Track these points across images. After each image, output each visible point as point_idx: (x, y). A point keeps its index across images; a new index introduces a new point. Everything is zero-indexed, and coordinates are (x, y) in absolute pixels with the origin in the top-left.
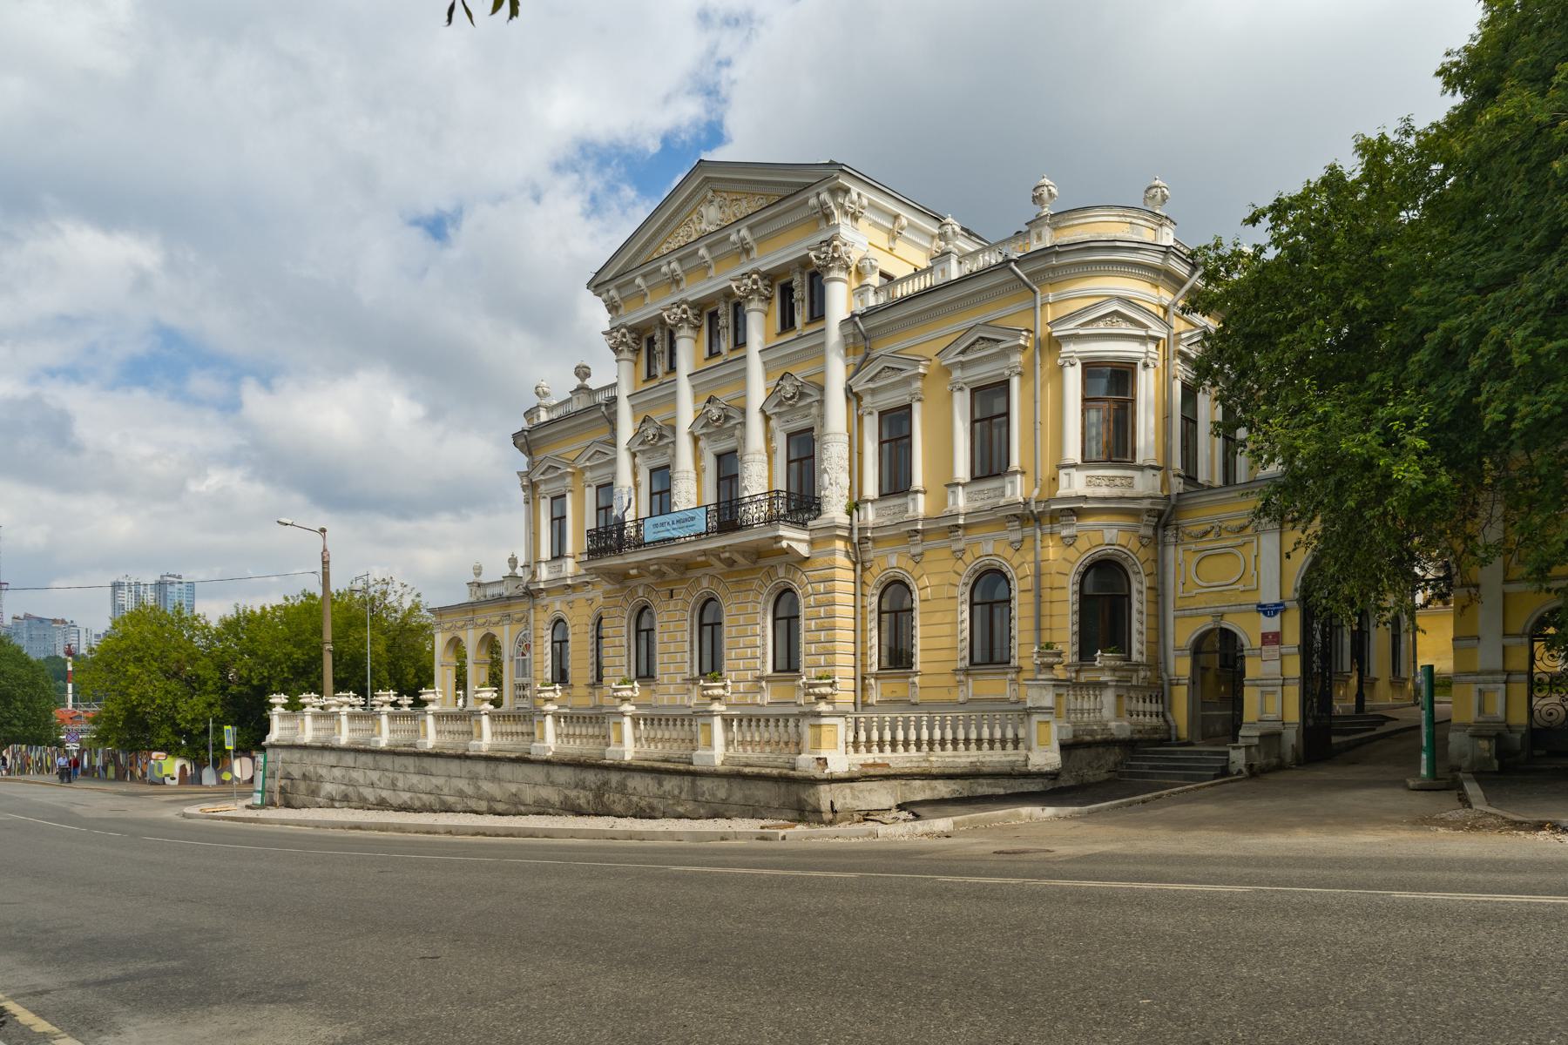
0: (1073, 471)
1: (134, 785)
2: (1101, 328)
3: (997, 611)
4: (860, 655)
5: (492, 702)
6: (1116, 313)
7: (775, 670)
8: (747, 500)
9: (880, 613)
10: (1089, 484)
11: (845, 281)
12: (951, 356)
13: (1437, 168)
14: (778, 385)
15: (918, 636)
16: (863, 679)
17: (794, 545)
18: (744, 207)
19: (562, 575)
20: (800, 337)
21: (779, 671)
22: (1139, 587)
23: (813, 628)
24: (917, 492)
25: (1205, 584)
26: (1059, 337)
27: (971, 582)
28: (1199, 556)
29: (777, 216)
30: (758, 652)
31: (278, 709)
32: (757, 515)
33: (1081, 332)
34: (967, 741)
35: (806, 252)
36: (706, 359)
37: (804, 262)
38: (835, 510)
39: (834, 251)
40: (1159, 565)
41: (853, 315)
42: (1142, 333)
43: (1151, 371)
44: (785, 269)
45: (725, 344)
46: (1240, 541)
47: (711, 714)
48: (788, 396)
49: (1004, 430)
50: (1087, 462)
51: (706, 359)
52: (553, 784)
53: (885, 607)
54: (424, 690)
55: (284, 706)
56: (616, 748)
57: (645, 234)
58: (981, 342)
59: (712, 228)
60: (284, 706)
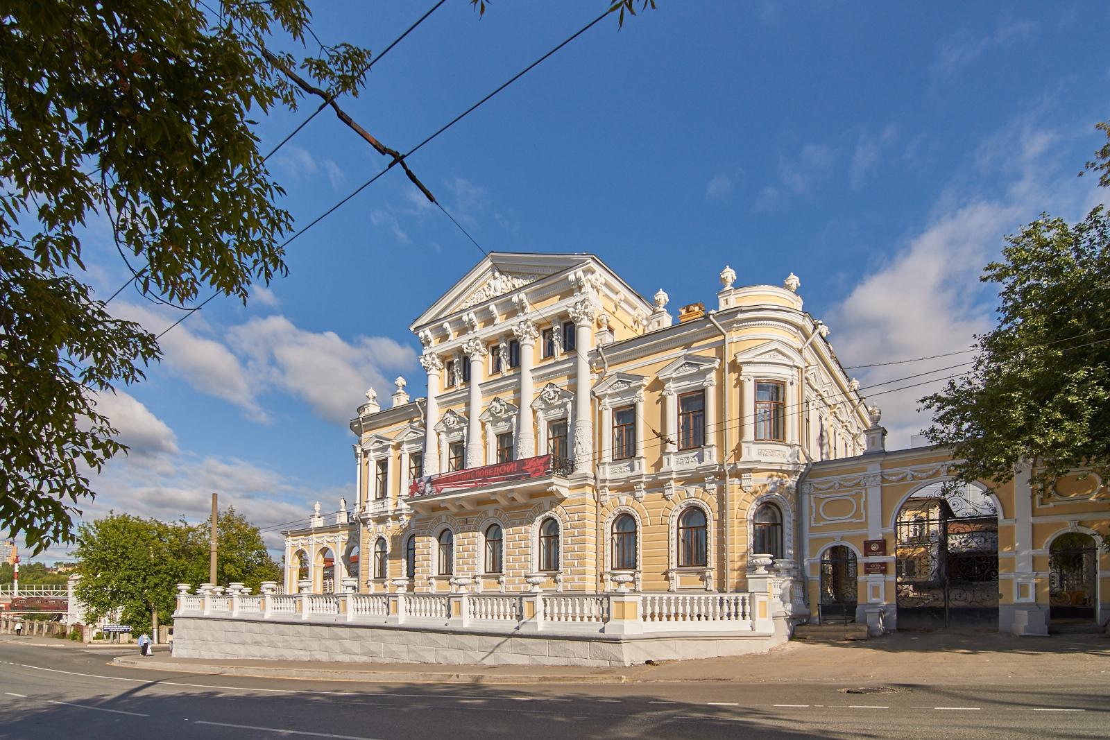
0: (751, 444)
1: (50, 640)
2: (766, 358)
4: (599, 559)
5: (354, 588)
6: (776, 350)
7: (678, 566)
10: (760, 453)
11: (590, 328)
13: (65, 426)
16: (602, 575)
17: (559, 488)
18: (519, 283)
19: (385, 509)
20: (557, 363)
21: (615, 569)
22: (789, 519)
24: (670, 453)
31: (184, 592)
33: (756, 361)
34: (676, 615)
35: (566, 308)
37: (563, 316)
38: (584, 466)
39: (585, 308)
43: (794, 386)
44: (550, 321)
47: (461, 596)
49: (632, 432)
51: (446, 389)
53: (681, 526)
55: (188, 591)
56: (455, 619)
57: (451, 296)
59: (498, 294)
60: (188, 591)
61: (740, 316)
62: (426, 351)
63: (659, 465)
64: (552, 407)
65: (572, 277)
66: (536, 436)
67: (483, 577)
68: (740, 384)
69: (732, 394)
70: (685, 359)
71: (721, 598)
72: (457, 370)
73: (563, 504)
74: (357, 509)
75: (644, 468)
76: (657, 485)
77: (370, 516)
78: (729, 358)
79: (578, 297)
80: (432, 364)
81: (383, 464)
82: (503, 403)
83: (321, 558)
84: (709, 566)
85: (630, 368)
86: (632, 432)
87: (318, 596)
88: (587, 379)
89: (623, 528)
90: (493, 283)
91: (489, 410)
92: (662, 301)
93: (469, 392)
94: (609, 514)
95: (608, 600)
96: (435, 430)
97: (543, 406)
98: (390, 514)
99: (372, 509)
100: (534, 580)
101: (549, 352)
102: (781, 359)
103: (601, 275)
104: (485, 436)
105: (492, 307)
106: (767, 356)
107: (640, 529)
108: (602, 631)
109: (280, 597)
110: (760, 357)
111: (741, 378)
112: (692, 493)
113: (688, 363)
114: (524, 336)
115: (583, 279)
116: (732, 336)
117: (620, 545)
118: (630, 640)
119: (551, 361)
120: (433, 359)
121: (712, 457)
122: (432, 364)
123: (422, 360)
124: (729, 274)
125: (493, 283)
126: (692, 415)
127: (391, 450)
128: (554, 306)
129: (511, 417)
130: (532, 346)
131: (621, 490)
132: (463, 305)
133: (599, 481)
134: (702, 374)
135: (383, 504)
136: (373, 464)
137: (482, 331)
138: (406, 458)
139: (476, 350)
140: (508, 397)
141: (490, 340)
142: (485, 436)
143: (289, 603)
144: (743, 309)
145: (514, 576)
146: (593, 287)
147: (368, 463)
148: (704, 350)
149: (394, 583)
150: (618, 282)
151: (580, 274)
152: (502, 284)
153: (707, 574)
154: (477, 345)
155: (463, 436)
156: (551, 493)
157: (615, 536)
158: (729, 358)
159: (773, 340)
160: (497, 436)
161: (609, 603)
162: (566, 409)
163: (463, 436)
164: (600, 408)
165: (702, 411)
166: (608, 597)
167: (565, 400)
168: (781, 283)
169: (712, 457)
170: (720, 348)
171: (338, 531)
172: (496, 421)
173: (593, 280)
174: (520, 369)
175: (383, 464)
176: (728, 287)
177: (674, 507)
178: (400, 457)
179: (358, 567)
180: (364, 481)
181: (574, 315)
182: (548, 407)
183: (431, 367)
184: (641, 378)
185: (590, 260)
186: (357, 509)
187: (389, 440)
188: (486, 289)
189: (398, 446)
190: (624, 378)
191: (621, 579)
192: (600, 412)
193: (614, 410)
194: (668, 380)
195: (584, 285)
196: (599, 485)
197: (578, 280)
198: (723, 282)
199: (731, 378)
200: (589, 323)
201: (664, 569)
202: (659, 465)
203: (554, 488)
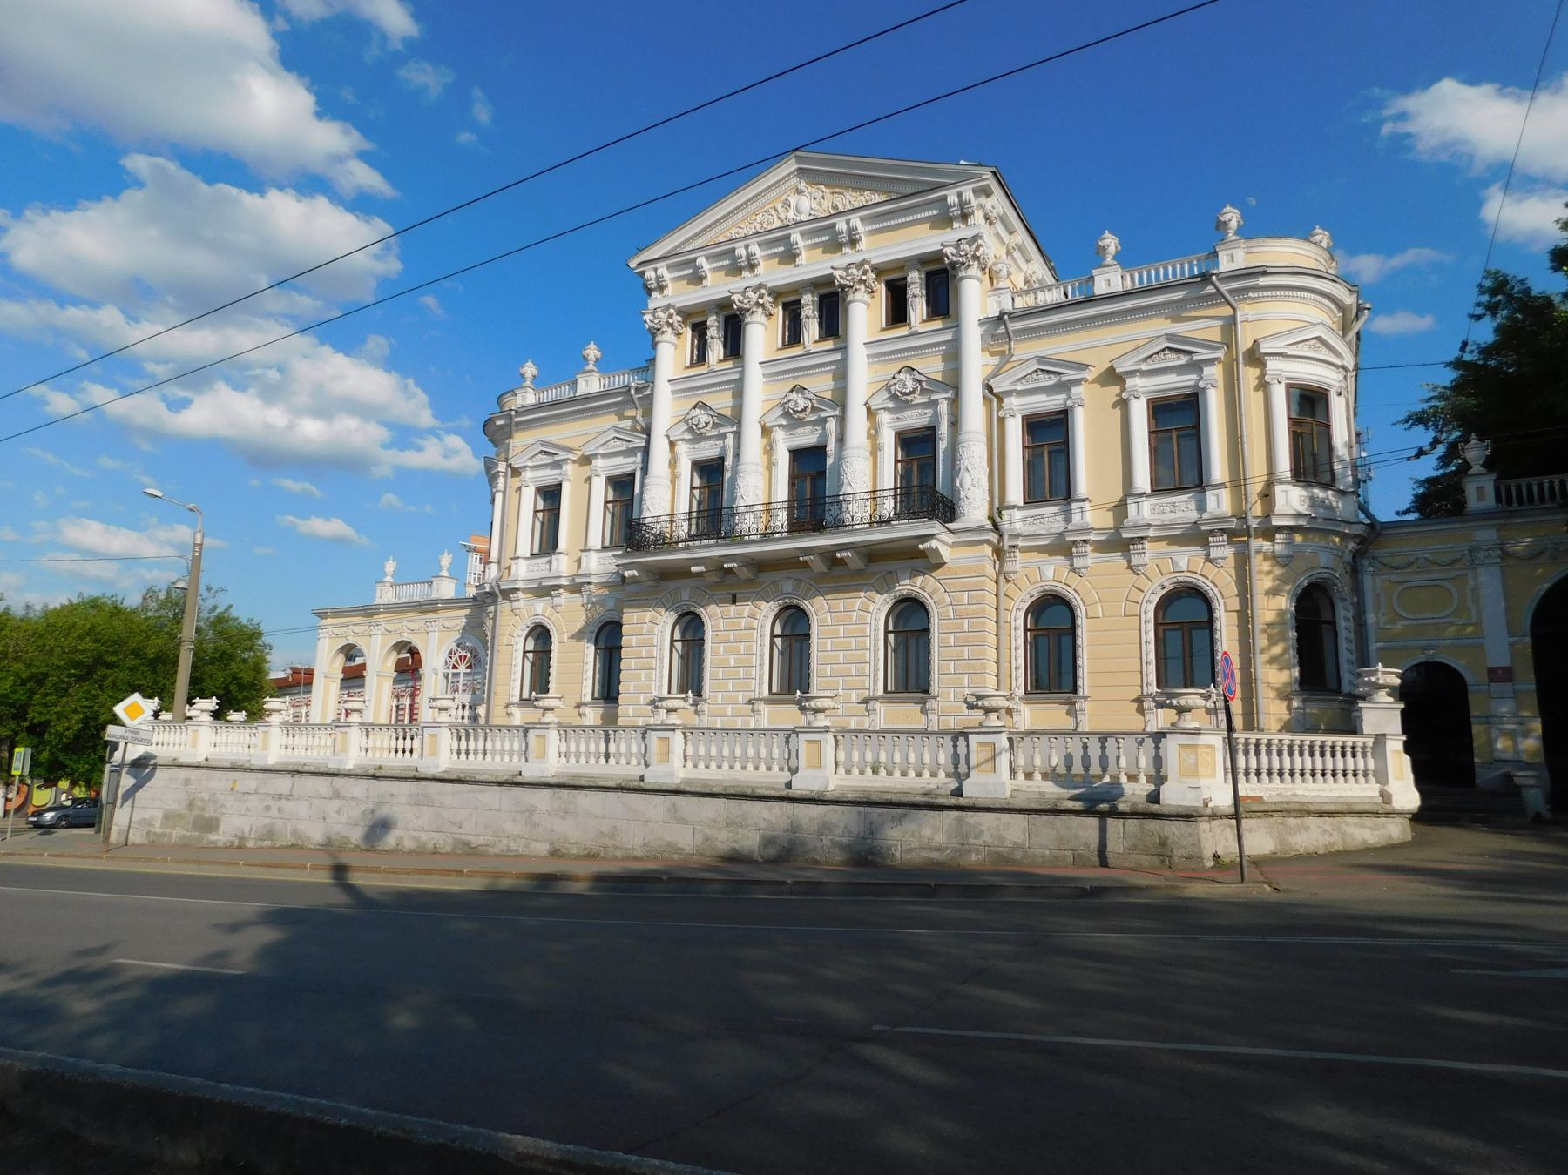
3: (912, 642)
6: (1319, 338)
8: (742, 509)
9: (1026, 630)
12: (522, 461)
14: (894, 378)
15: (1085, 657)
18: (850, 199)
20: (913, 335)
23: (644, 655)
25: (1412, 617)
26: (1200, 361)
27: (596, 631)
28: (1401, 587)
29: (926, 204)
30: (654, 675)
32: (859, 515)
36: (688, 368)
38: (975, 508)
40: (1358, 589)
41: (1002, 314)
42: (1338, 362)
44: (903, 265)
45: (716, 350)
46: (1452, 574)
48: (799, 409)
49: (630, 507)
50: (1159, 489)
51: (688, 368)
52: (684, 822)
54: (268, 699)
58: (616, 440)
61: (1262, 281)
62: (657, 301)
63: (1120, 509)
64: (907, 405)
65: (952, 198)
66: (673, 482)
67: (767, 701)
68: (1263, 385)
69: (1252, 402)
70: (1039, 362)
71: (1258, 740)
72: (714, 332)
73: (938, 573)
74: (493, 571)
75: (1092, 516)
76: (1120, 543)
77: (520, 585)
78: (1244, 343)
79: (960, 231)
80: (667, 323)
81: (551, 495)
82: (812, 396)
83: (340, 661)
84: (1080, 692)
85: (1061, 350)
86: (1061, 458)
87: (380, 727)
88: (976, 364)
89: (792, 630)
90: (793, 200)
91: (782, 405)
92: (529, 375)
93: (742, 373)
94: (1018, 596)
95: (967, 740)
96: (668, 436)
97: (784, 422)
98: (564, 582)
99: (525, 571)
100: (439, 704)
101: (700, 357)
102: (1324, 354)
103: (997, 203)
104: (673, 463)
105: (796, 237)
106: (1305, 346)
107: (1083, 623)
108: (789, 785)
109: (294, 726)
110: (1291, 347)
111: (1267, 378)
112: (1183, 564)
113: (1170, 349)
114: (857, 286)
115: (974, 202)
116: (1246, 311)
117: (901, 651)
118: (177, 765)
119: (903, 331)
120: (671, 316)
121: (1220, 503)
122: (667, 323)
123: (648, 317)
124: (1232, 216)
125: (793, 200)
126: (1175, 434)
127: (569, 468)
128: (920, 240)
129: (824, 421)
130: (865, 303)
131: (1050, 550)
132: (733, 231)
133: (1006, 537)
134: (1196, 367)
135: (550, 563)
136: (529, 494)
137: (774, 274)
138: (599, 484)
139: (758, 304)
140: (822, 385)
141: (780, 290)
142: (673, 463)
143: (324, 738)
144: (1269, 270)
145: (726, 702)
146: (987, 218)
147: (519, 489)
148: (1203, 327)
149: (434, 704)
150: (1016, 215)
151: (968, 194)
152: (808, 202)
153: (1078, 706)
154: (865, 273)
155: (724, 449)
156: (923, 554)
157: (891, 637)
158: (1244, 343)
159: (1312, 324)
160: (790, 451)
161: (968, 746)
162: (936, 412)
163: (724, 449)
164: (1001, 414)
165: (1195, 432)
166: (965, 735)
167: (723, 430)
168: (1306, 237)
169: (1220, 503)
170: (1230, 324)
171: (435, 611)
172: (697, 436)
173: (988, 207)
174: (743, 362)
175: (551, 495)
176: (591, 366)
177: (1148, 587)
178: (589, 480)
179: (312, 678)
180: (511, 521)
181: (843, 282)
182: (900, 402)
183: (665, 328)
184: (1083, 367)
185: (990, 175)
186: (493, 571)
187: (570, 450)
188: (779, 209)
189: (586, 460)
190: (1048, 365)
191: (1183, 702)
192: (1002, 420)
193: (1025, 418)
194: (595, 456)
195: (860, 239)
196: (1007, 543)
197: (963, 204)
198: (1221, 226)
199: (1249, 375)
200: (979, 274)
201: (1136, 693)
202: (1120, 509)
203: (933, 544)
